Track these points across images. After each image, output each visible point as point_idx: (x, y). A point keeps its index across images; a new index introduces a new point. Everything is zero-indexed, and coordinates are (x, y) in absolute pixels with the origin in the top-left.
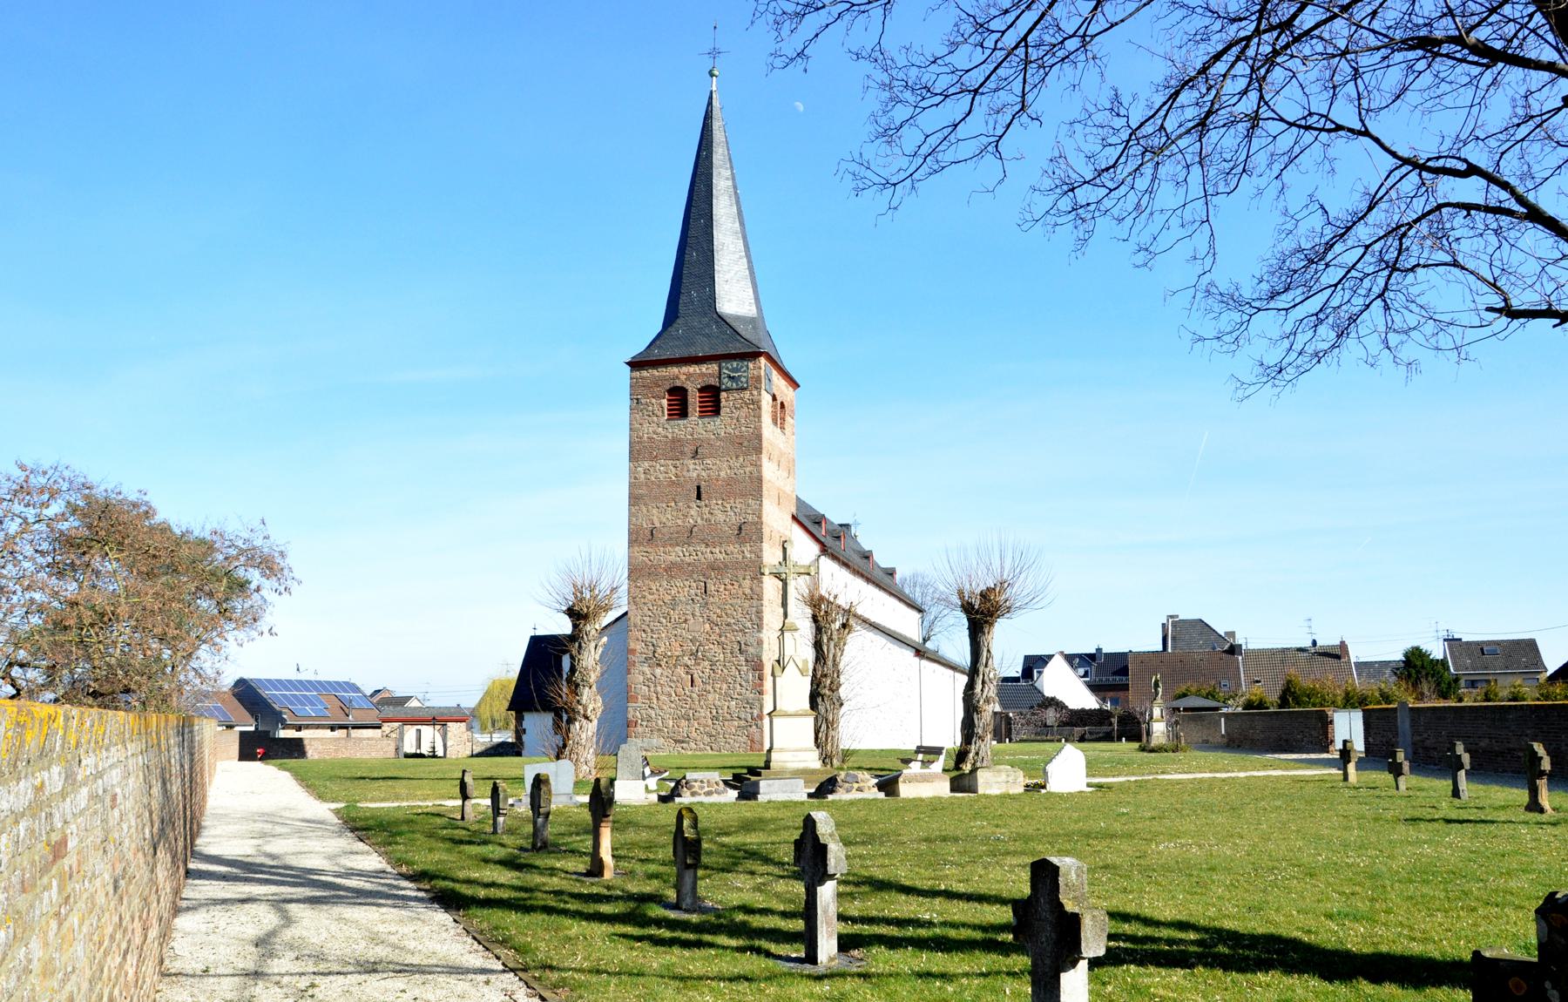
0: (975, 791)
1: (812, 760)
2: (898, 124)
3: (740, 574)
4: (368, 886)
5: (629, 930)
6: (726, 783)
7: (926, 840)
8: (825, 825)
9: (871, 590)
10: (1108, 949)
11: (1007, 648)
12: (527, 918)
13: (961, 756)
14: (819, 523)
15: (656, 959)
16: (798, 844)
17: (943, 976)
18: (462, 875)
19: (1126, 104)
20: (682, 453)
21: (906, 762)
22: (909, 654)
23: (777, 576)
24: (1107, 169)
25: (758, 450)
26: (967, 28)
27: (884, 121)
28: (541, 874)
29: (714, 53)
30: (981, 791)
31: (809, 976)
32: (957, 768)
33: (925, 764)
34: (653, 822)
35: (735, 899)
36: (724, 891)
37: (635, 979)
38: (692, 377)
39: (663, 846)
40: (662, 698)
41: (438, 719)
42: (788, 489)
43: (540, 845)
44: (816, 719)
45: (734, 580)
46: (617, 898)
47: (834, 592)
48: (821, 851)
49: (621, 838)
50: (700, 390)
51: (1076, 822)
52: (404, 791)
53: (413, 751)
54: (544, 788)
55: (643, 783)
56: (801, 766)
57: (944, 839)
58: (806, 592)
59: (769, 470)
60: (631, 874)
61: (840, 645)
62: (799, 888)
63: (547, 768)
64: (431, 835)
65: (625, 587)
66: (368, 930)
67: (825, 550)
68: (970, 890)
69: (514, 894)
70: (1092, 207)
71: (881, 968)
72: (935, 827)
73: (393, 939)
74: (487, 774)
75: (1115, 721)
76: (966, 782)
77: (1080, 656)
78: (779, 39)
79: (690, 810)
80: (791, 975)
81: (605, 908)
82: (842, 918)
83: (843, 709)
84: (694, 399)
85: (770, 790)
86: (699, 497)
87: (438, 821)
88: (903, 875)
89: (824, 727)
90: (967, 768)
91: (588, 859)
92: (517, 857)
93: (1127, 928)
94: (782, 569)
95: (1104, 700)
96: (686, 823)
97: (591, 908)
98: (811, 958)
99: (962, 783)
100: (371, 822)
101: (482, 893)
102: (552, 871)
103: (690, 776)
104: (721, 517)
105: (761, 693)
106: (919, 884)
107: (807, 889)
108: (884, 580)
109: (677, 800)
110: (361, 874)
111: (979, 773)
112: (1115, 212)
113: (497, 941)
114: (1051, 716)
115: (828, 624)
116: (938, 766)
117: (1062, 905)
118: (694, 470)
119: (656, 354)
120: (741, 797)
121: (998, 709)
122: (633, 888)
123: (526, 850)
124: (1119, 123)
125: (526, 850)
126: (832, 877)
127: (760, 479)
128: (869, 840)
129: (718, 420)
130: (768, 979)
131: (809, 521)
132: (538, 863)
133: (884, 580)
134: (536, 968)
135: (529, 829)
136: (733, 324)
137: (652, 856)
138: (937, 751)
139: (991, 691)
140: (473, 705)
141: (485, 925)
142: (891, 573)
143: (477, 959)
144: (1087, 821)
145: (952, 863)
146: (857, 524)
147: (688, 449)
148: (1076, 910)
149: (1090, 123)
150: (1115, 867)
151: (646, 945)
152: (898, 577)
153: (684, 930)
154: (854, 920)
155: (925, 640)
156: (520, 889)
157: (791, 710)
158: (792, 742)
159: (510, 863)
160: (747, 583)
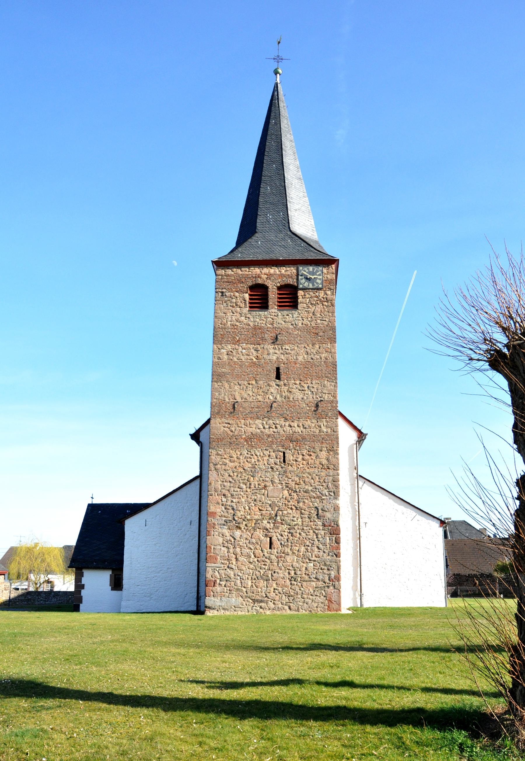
86: (278, 377)
118: (273, 354)
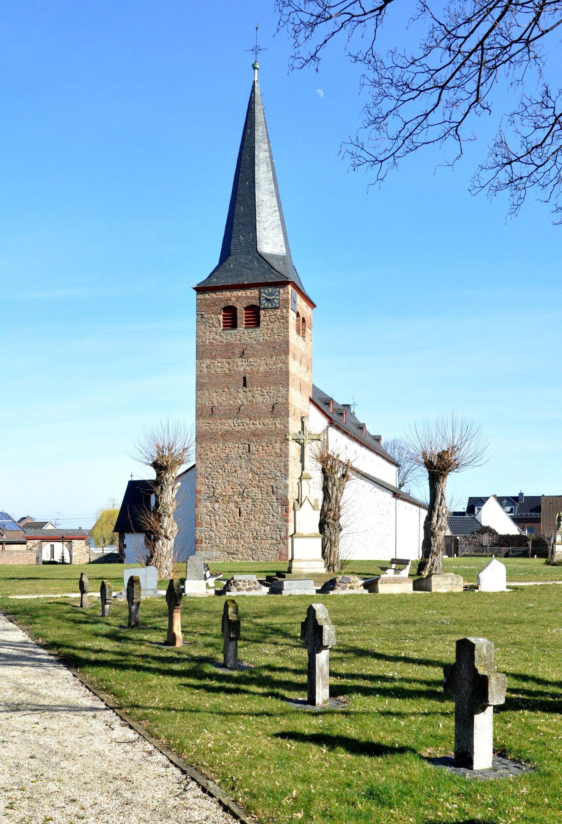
0: (430, 590)
1: (320, 568)
2: (385, 113)
3: (273, 439)
4: (15, 653)
5: (191, 681)
6: (261, 582)
7: (395, 623)
8: (322, 613)
9: (364, 451)
10: (507, 699)
11: (456, 492)
12: (123, 674)
13: (422, 566)
14: (328, 404)
15: (208, 701)
16: (304, 625)
17: (398, 715)
18: (79, 644)
19: (553, 98)
20: (233, 354)
21: (384, 569)
22: (388, 496)
23: (297, 441)
24: (537, 147)
25: (286, 352)
26: (439, 34)
27: (374, 111)
28: (133, 643)
29: (256, 50)
30: (434, 590)
31: (309, 713)
32: (419, 573)
33: (397, 571)
34: (211, 609)
35: (263, 661)
36: (254, 656)
37: (193, 714)
38: (240, 299)
39: (217, 625)
40: (220, 524)
41: (66, 538)
42: (307, 380)
43: (134, 623)
44: (323, 540)
45: (269, 443)
46: (184, 660)
47: (337, 453)
48: (319, 629)
49: (188, 619)
50: (246, 309)
51: (497, 612)
52: (41, 588)
53: (48, 559)
54: (136, 586)
55: (204, 583)
56: (313, 571)
57: (407, 622)
58: (318, 453)
59: (294, 366)
60: (194, 644)
61: (341, 489)
62: (305, 653)
63: (139, 572)
64: (59, 618)
65: (193, 448)
66: (14, 682)
67: (332, 423)
68: (421, 657)
69: (114, 657)
70: (525, 179)
71: (358, 708)
72: (401, 614)
73: (31, 687)
74: (99, 576)
75: (530, 543)
76: (424, 583)
77: (508, 498)
78: (297, 45)
79: (233, 601)
80: (297, 712)
81: (176, 667)
82: (332, 674)
83: (342, 533)
84: (241, 315)
85: (291, 588)
86: (245, 385)
87: (65, 608)
88: (377, 646)
89: (329, 545)
90: (425, 574)
91: (165, 633)
92: (117, 632)
93: (525, 685)
94: (301, 437)
95: (523, 529)
96: (230, 610)
97: (166, 666)
98: (312, 701)
99: (421, 584)
100: (18, 609)
101: (93, 657)
102: (141, 642)
103: (237, 577)
104: (260, 399)
105: (287, 521)
106: (387, 652)
107: (309, 655)
108: (373, 444)
109: (228, 593)
110: (10, 644)
111: (433, 578)
112: (541, 182)
113: (102, 689)
114: (486, 539)
115: (333, 475)
116: (405, 573)
117: (476, 670)
118: (241, 366)
119: (215, 282)
120: (272, 592)
121: (448, 533)
122: (195, 653)
123: (123, 627)
124: (548, 113)
125: (123, 627)
126: (326, 647)
127: (287, 373)
128: (355, 622)
129: (258, 330)
130: (282, 714)
131: (322, 402)
132: (132, 636)
133: (373, 444)
134: (127, 707)
135: (126, 613)
136: (270, 261)
137: (209, 632)
138: (405, 562)
139: (444, 522)
140: (90, 528)
141: (94, 678)
142: (378, 439)
143: (88, 701)
144: (502, 614)
145: (411, 639)
146: (355, 405)
147: (238, 351)
148: (486, 673)
149: (526, 114)
150: (521, 644)
151: (202, 691)
152: (382, 442)
153: (228, 682)
154: (342, 676)
155: (401, 486)
156: (120, 654)
157: (306, 533)
158: (307, 555)
159: (113, 636)
160: (278, 445)
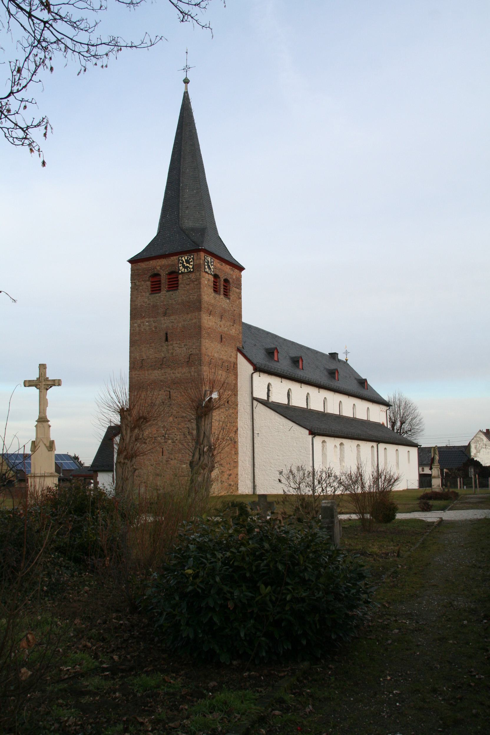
29: (187, 69)
86: (167, 340)
118: (165, 323)
129: (177, 293)
147: (161, 311)
